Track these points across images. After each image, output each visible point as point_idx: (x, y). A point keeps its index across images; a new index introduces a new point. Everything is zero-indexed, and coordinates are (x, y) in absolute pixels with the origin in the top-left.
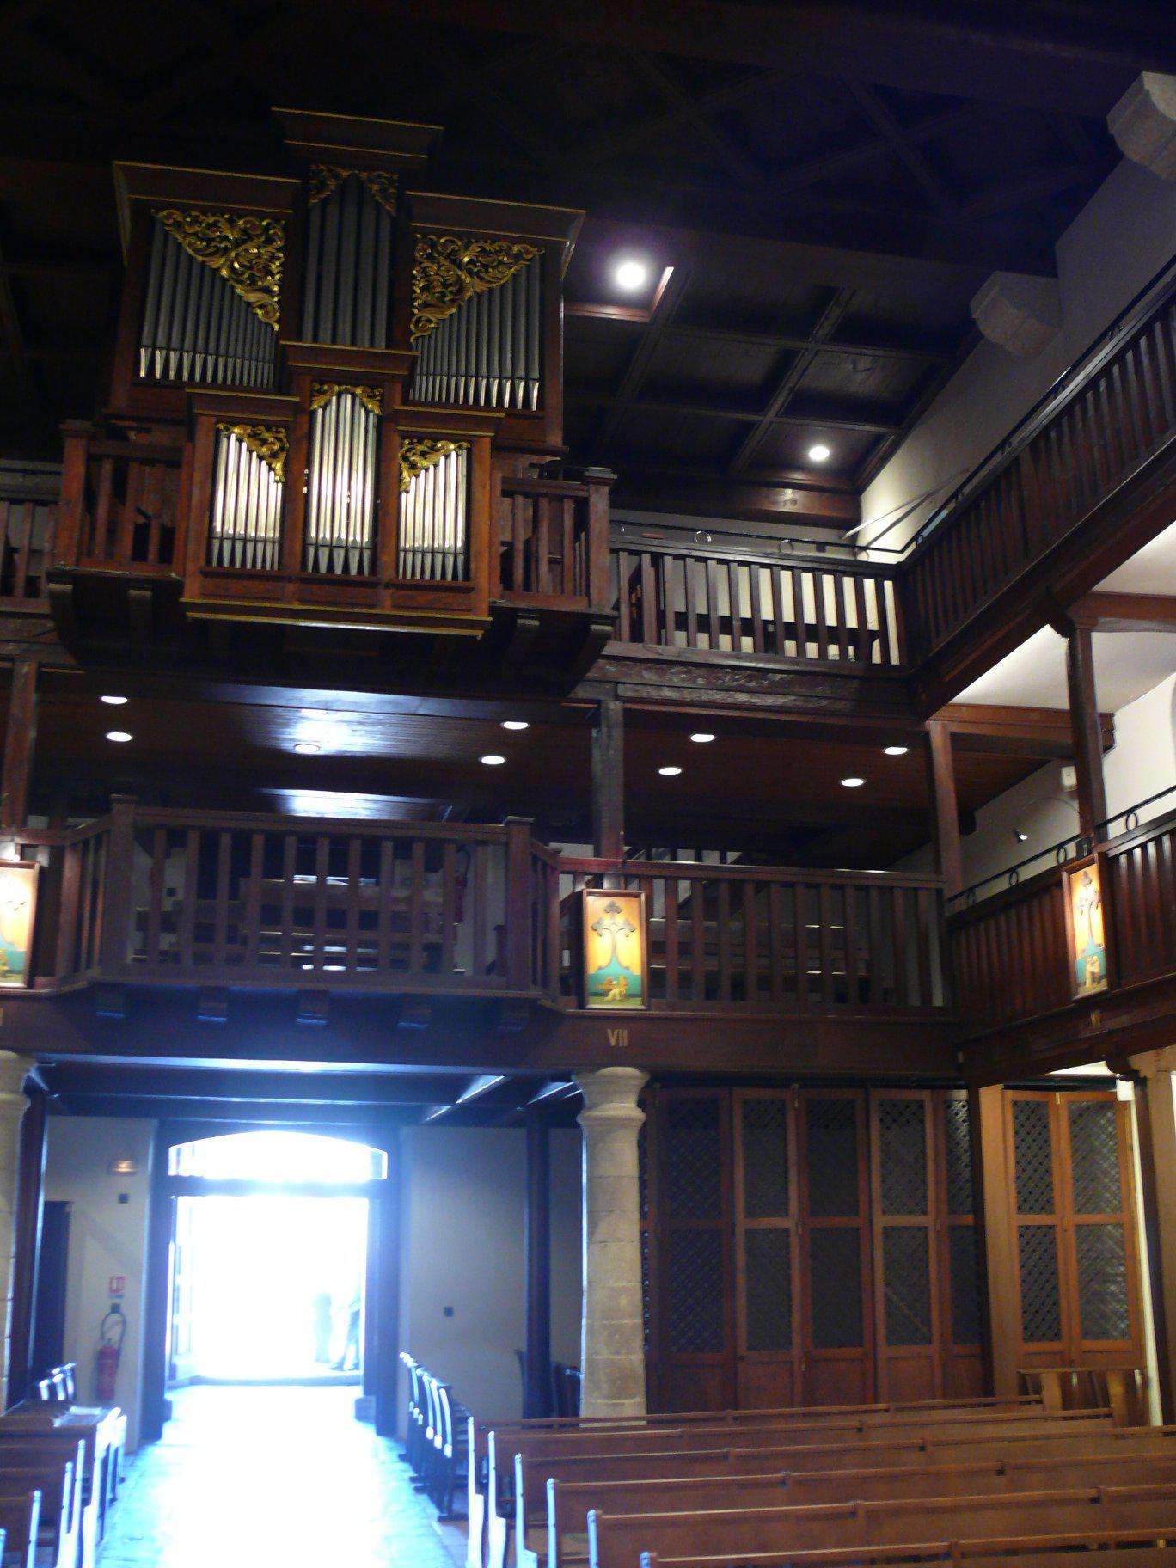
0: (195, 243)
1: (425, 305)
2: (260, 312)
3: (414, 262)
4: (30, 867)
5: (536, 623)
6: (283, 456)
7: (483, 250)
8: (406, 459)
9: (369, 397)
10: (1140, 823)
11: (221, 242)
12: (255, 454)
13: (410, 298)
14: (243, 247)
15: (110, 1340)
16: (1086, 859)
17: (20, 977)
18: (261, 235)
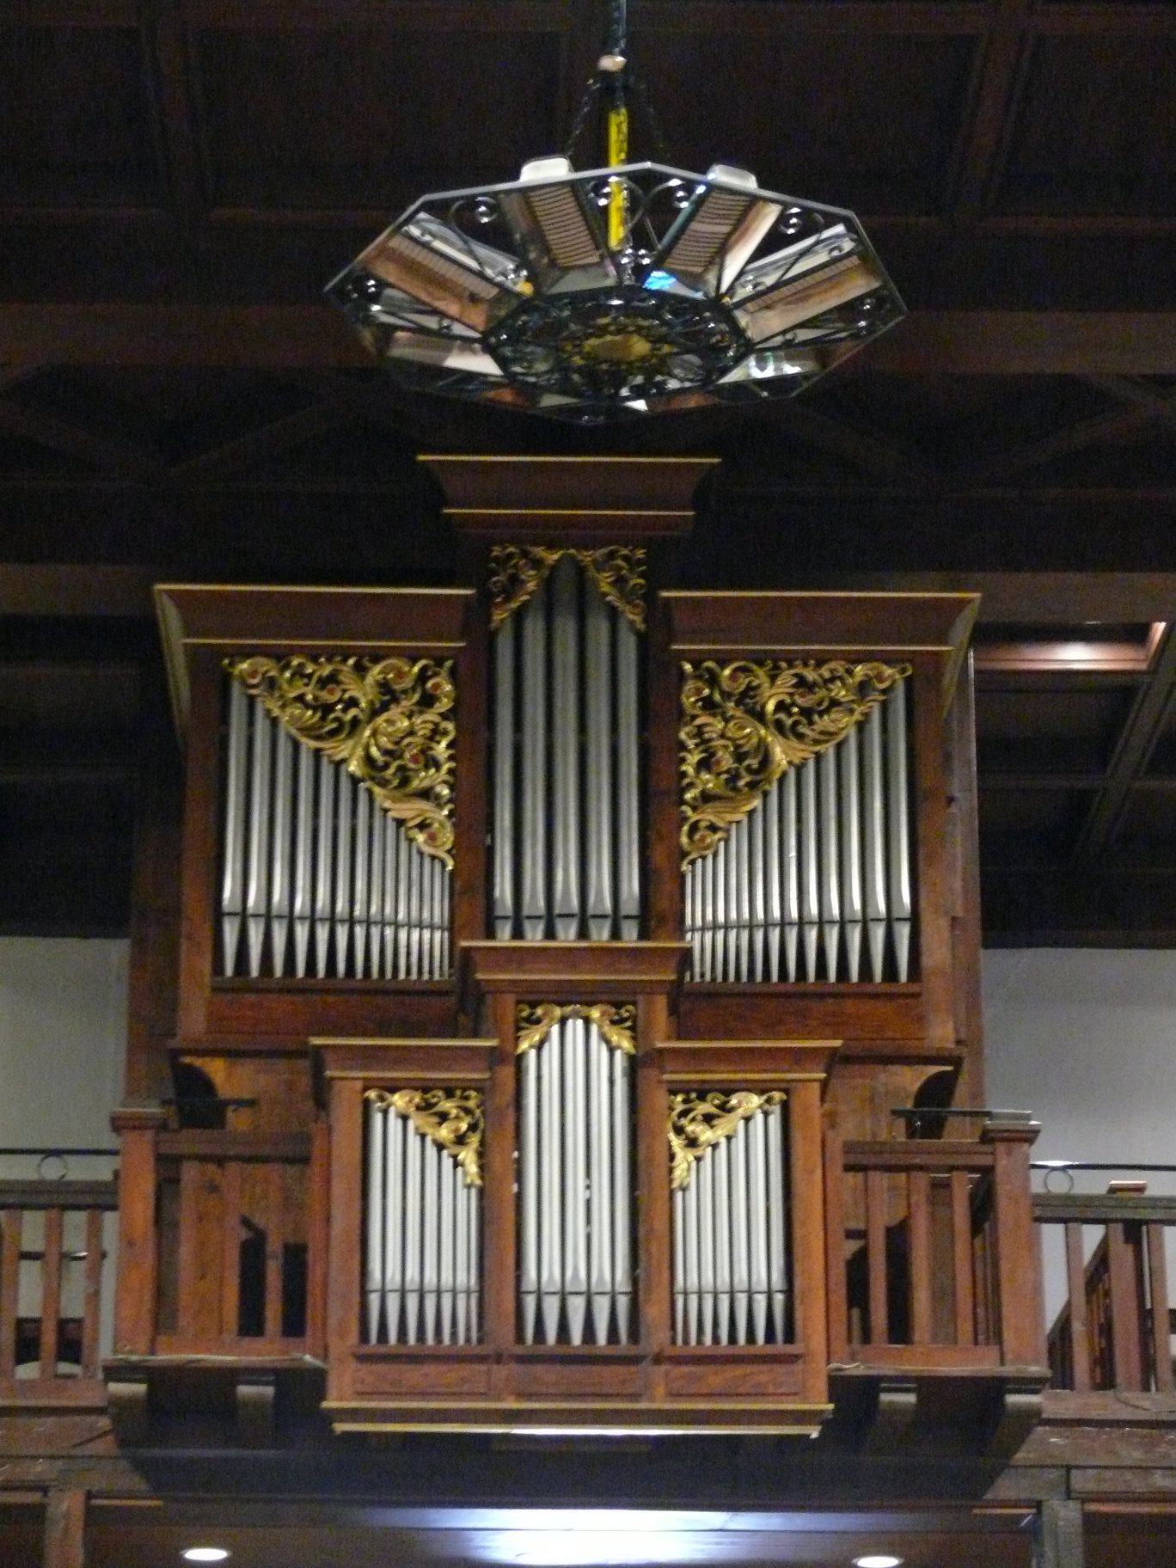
0: (303, 715)
1: (706, 797)
2: (421, 838)
3: (681, 716)
5: (911, 1398)
6: (474, 1140)
7: (802, 682)
9: (613, 1022)
11: (345, 710)
12: (429, 1140)
14: (385, 716)
18: (413, 689)
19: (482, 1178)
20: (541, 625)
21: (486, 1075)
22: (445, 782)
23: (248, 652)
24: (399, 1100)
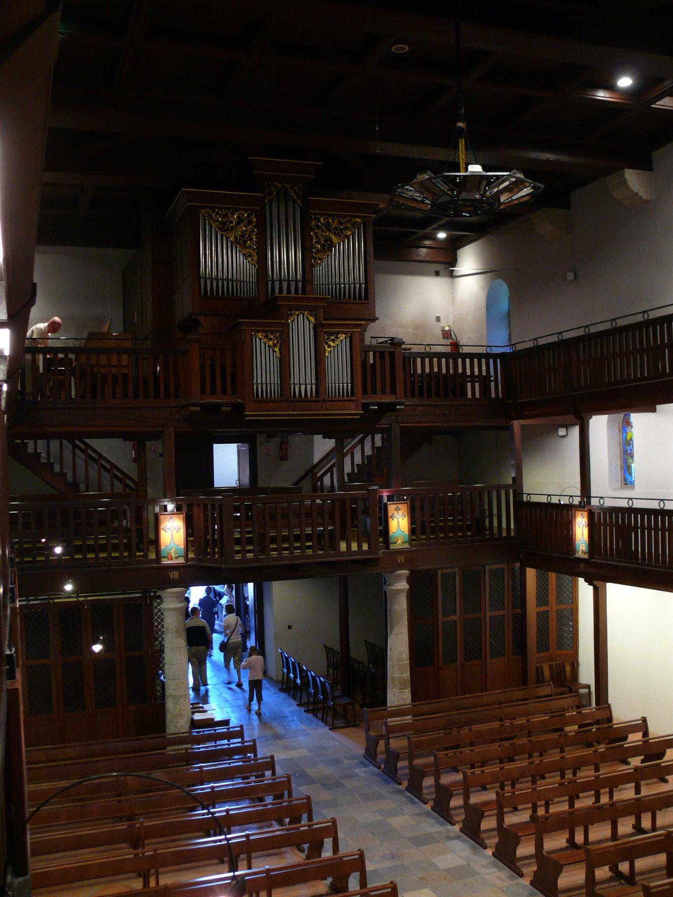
8: (327, 343)
12: (267, 345)
19: (280, 355)
20: (284, 204)
21: (281, 329)
22: (255, 244)
23: (205, 208)
24: (260, 335)
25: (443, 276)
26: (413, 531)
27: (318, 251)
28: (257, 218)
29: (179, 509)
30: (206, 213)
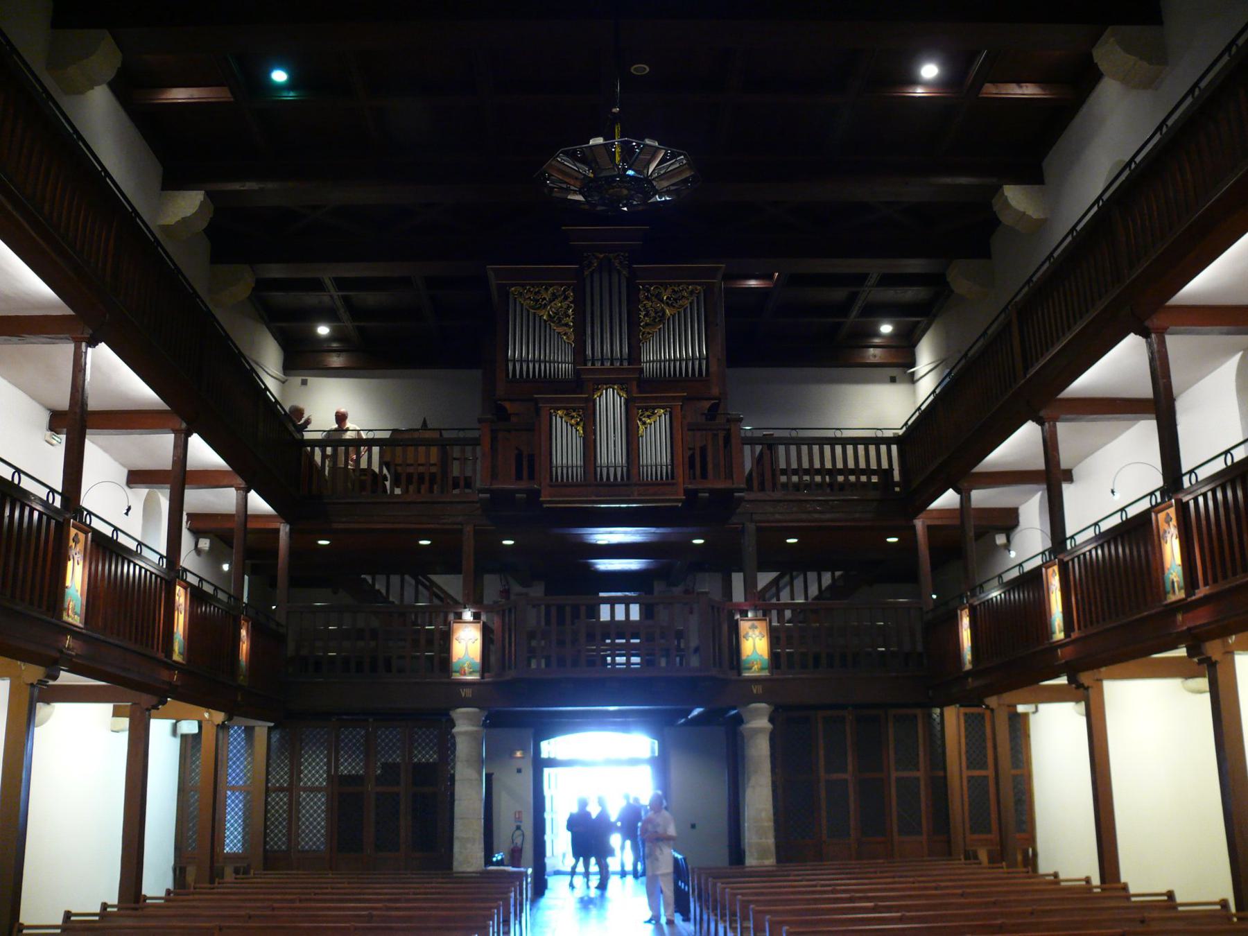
1: (647, 324)
3: (639, 301)
4: (479, 623)
6: (582, 424)
7: (674, 291)
8: (640, 420)
10: (1199, 479)
13: (639, 320)
15: (516, 844)
16: (1168, 503)
17: (478, 674)
23: (513, 285)
25: (902, 382)
26: (774, 656)
27: (647, 324)
28: (573, 293)
29: (476, 617)
30: (516, 291)
